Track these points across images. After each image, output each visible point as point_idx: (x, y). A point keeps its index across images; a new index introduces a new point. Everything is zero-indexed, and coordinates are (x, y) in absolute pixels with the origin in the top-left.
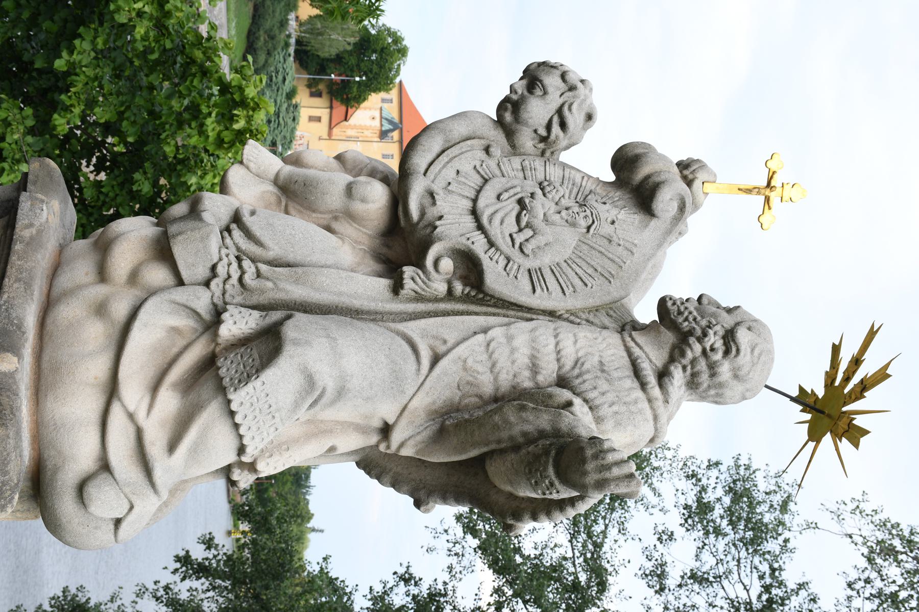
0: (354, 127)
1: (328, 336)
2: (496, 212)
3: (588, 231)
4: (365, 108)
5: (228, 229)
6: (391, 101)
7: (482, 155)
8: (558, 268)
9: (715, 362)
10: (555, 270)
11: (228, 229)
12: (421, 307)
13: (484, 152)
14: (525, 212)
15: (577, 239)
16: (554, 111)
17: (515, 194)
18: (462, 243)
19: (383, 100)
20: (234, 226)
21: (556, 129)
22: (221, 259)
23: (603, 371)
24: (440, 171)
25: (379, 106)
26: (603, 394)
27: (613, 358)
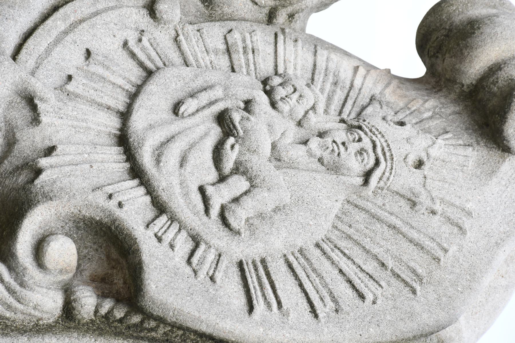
3: (366, 182)
8: (302, 260)
10: (295, 264)
15: (342, 197)
17: (212, 103)
24: (48, 51)
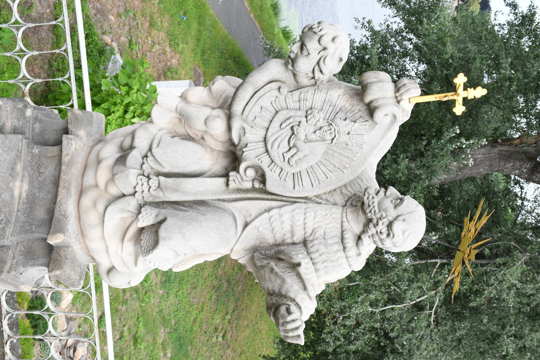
1: (181, 233)
3: (332, 142)
7: (276, 93)
8: (311, 170)
9: (382, 239)
10: (309, 172)
11: (146, 156)
12: (238, 196)
13: (278, 91)
14: (293, 136)
15: (325, 147)
16: (315, 63)
17: (290, 124)
18: (256, 162)
22: (138, 184)
23: (324, 239)
24: (252, 108)
26: (321, 255)
27: (332, 230)
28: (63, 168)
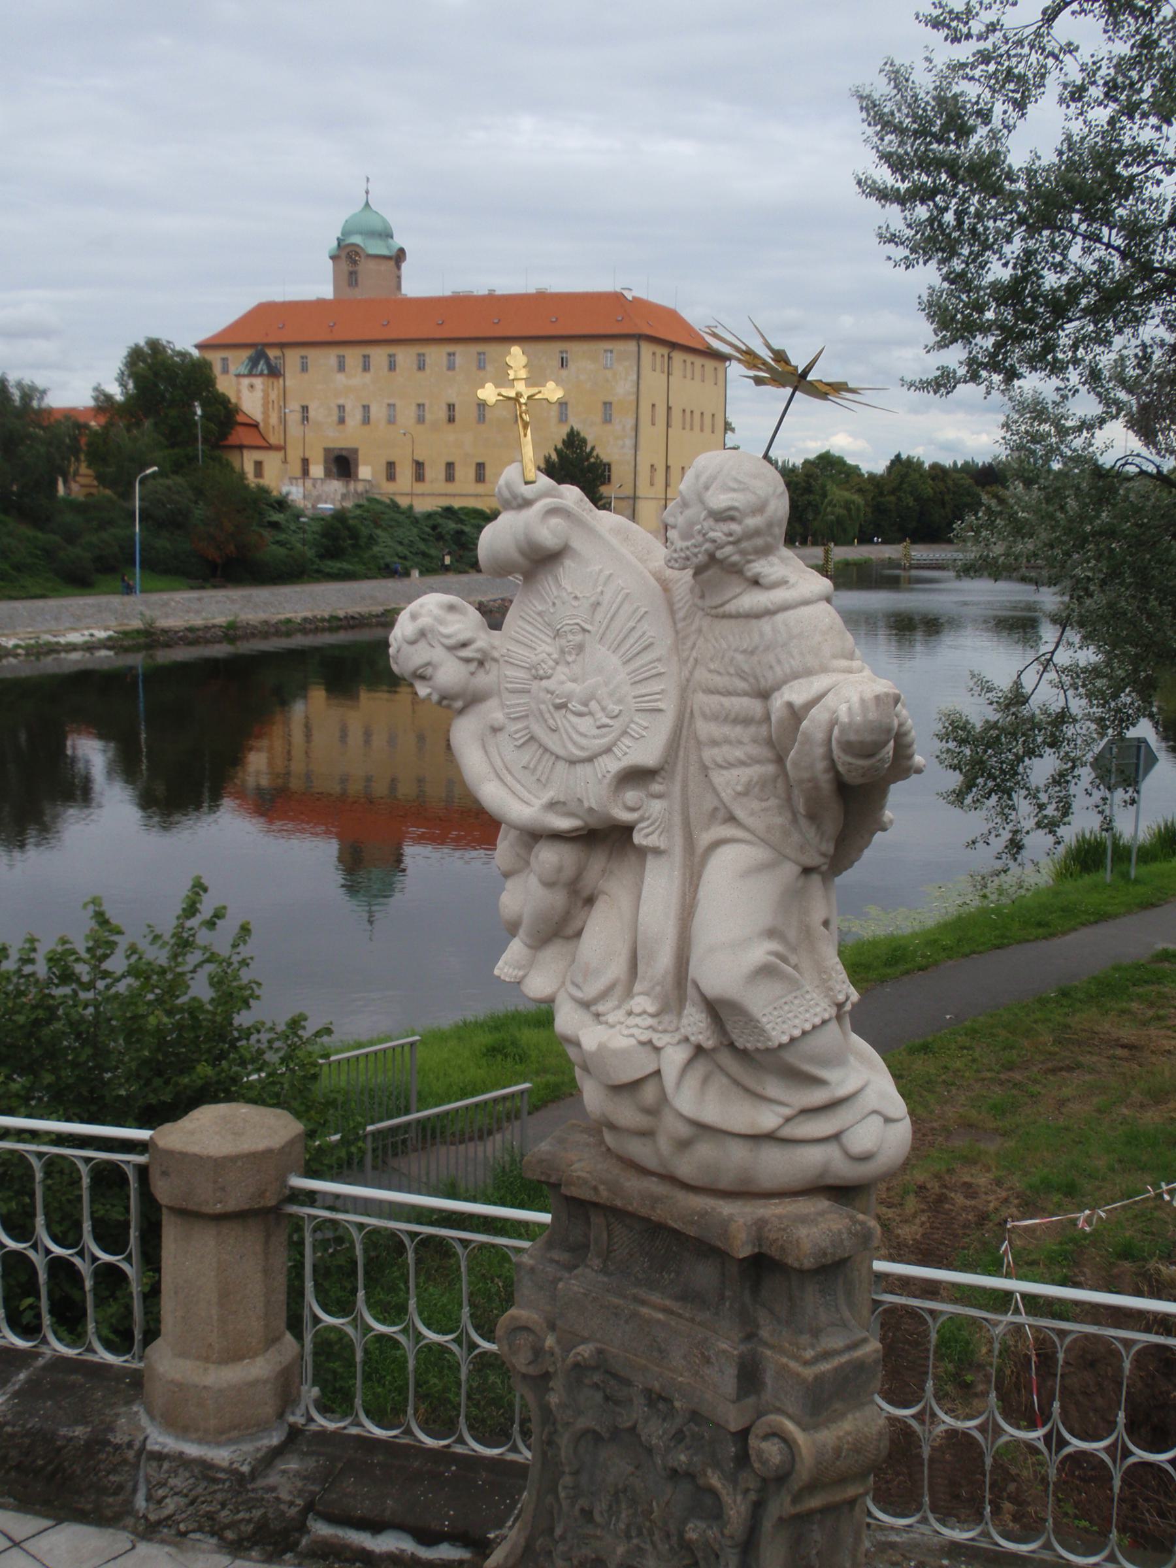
0: (266, 413)
2: (574, 743)
4: (239, 398)
5: (598, 1015)
6: (224, 360)
7: (502, 737)
11: (598, 1015)
13: (498, 734)
19: (225, 371)
20: (593, 1008)
21: (466, 653)
23: (752, 653)
25: (234, 379)
28: (619, 1203)
